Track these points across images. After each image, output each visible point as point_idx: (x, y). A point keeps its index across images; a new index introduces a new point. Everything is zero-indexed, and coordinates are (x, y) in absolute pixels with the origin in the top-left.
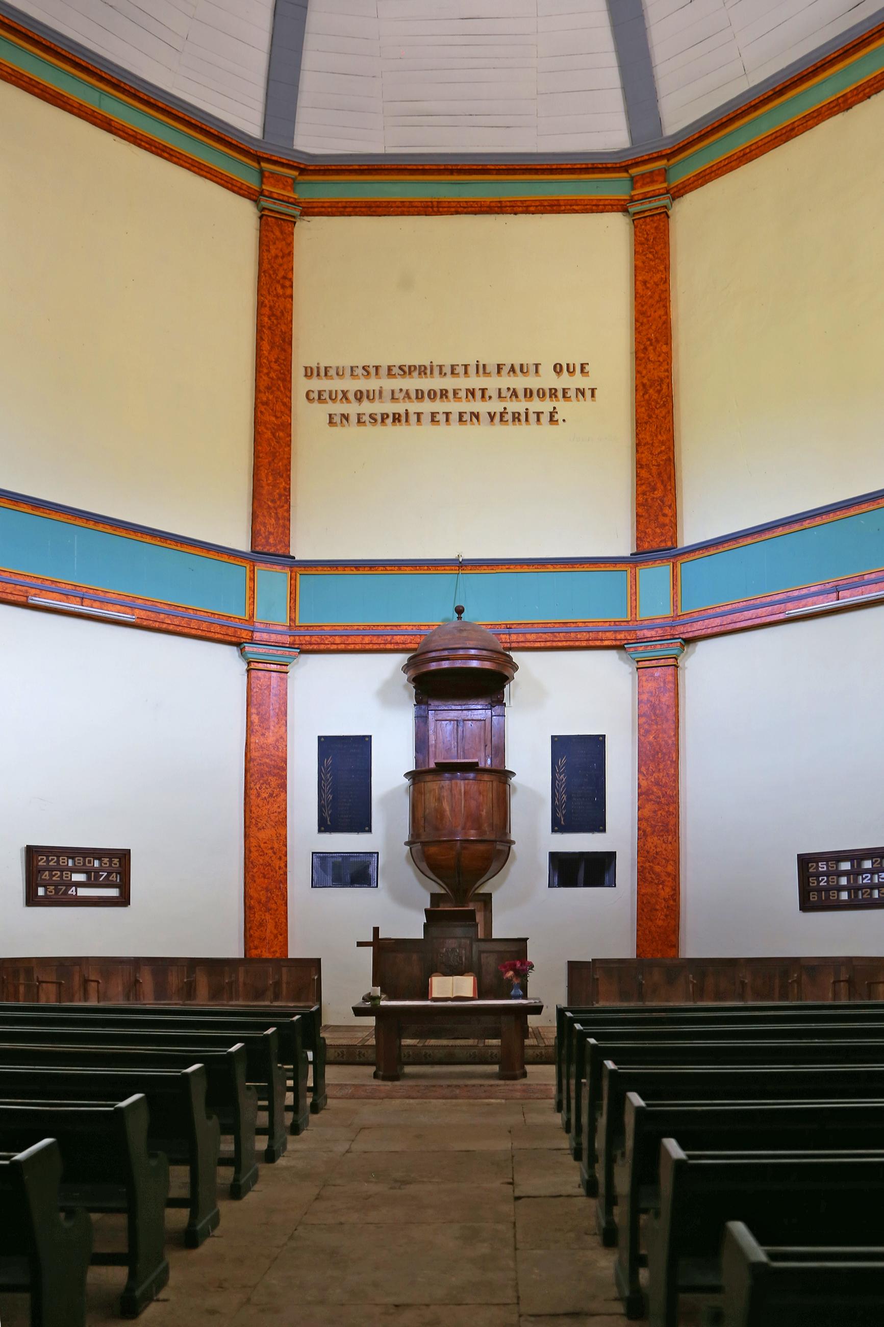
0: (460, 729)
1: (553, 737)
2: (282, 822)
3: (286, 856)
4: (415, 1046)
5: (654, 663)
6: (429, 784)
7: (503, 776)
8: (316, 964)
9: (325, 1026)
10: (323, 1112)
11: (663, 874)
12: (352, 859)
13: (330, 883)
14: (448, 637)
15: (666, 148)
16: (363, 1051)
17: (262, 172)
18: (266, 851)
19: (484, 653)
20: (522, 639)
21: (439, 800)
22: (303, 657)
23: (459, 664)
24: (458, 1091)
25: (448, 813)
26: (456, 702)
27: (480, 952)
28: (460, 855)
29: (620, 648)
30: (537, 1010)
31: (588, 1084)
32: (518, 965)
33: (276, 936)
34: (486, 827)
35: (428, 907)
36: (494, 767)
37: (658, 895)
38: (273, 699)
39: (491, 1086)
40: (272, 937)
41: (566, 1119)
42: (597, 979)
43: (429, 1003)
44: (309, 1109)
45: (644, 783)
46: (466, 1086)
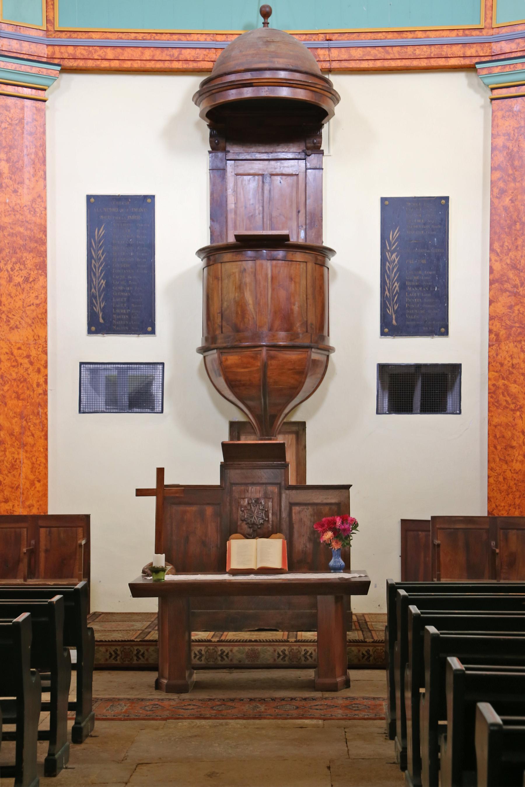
0: (267, 187)
1: (383, 200)
2: (42, 319)
3: (46, 367)
4: (209, 641)
5: (513, 91)
6: (228, 266)
7: (320, 254)
8: (84, 521)
9: (95, 613)
10: (88, 740)
12: (130, 373)
13: (103, 407)
14: (252, 52)
16: (142, 649)
18: (20, 360)
19: (297, 76)
20: (345, 57)
21: (240, 288)
22: (66, 77)
23: (265, 92)
24: (262, 708)
25: (251, 307)
26: (262, 149)
27: (292, 505)
28: (265, 364)
29: (471, 68)
30: (362, 587)
31: (427, 696)
32: (339, 522)
33: (32, 484)
34: (298, 328)
35: (226, 439)
36: (309, 243)
37: (514, 426)
38: (28, 140)
39: (305, 699)
40: (28, 485)
41: (400, 749)
42: (439, 545)
43: (226, 577)
44: (70, 737)
45: (497, 266)
46: (273, 699)
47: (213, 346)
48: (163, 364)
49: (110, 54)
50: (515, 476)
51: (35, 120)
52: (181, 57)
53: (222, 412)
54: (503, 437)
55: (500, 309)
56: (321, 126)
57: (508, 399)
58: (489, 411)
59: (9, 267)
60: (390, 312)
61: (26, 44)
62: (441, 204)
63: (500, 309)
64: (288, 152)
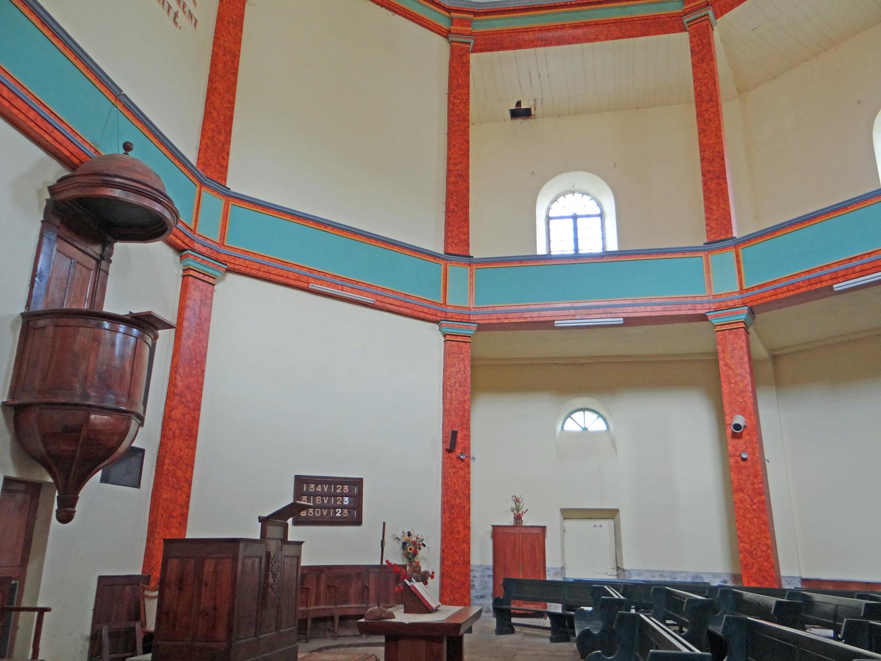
11: (182, 479)
17: (452, 19)
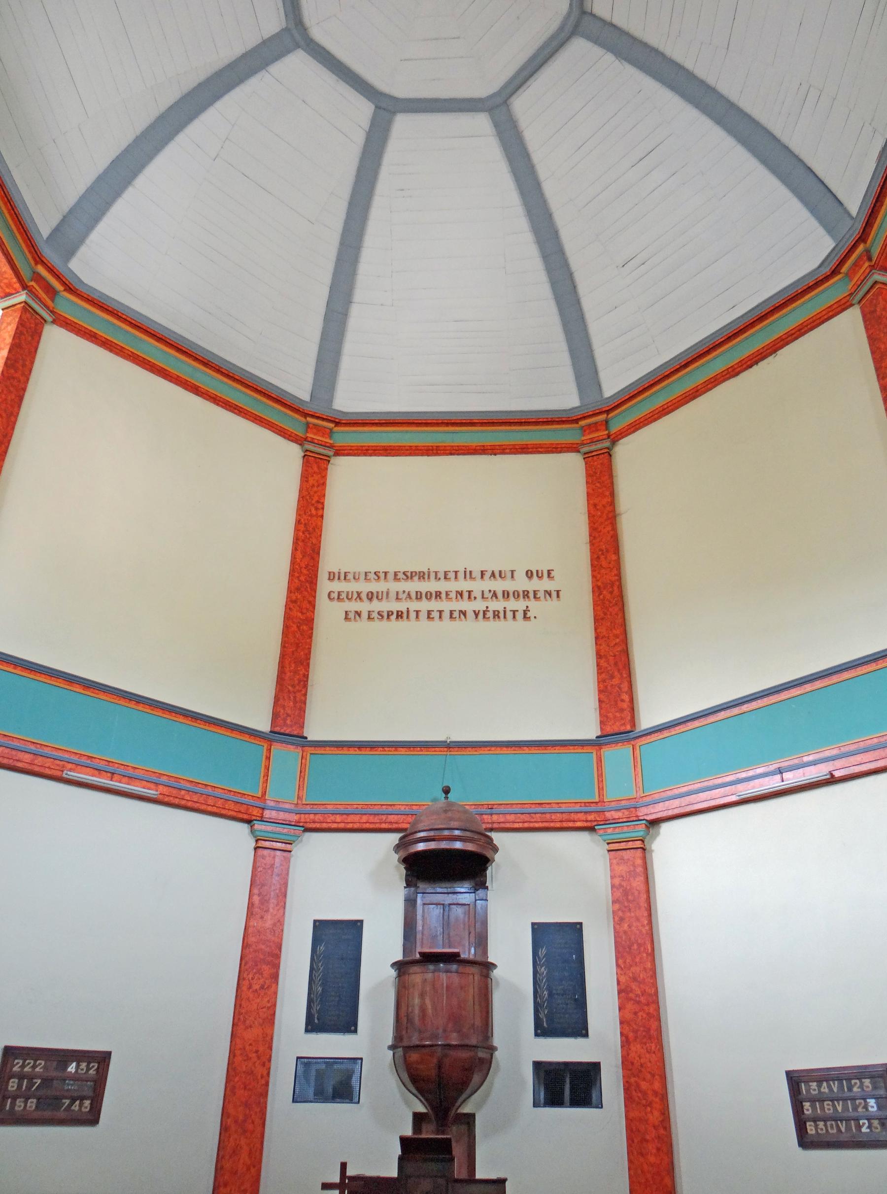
0: (446, 914)
1: (533, 924)
12: (335, 1067)
15: (855, 234)
19: (468, 834)
20: (502, 820)
22: (307, 834)
23: (444, 845)
26: (443, 885)
29: (591, 829)
33: (248, 1169)
35: (408, 1132)
38: (275, 879)
45: (623, 979)
47: (400, 1044)
48: (361, 1059)
49: (338, 818)
50: (651, 1169)
51: (281, 865)
52: (388, 820)
53: (407, 1103)
54: (639, 1131)
55: (629, 1016)
56: (485, 869)
57: (640, 1095)
58: (626, 1106)
59: (250, 976)
60: (541, 1016)
61: (281, 813)
62: (576, 929)
63: (629, 1016)
64: (463, 887)
